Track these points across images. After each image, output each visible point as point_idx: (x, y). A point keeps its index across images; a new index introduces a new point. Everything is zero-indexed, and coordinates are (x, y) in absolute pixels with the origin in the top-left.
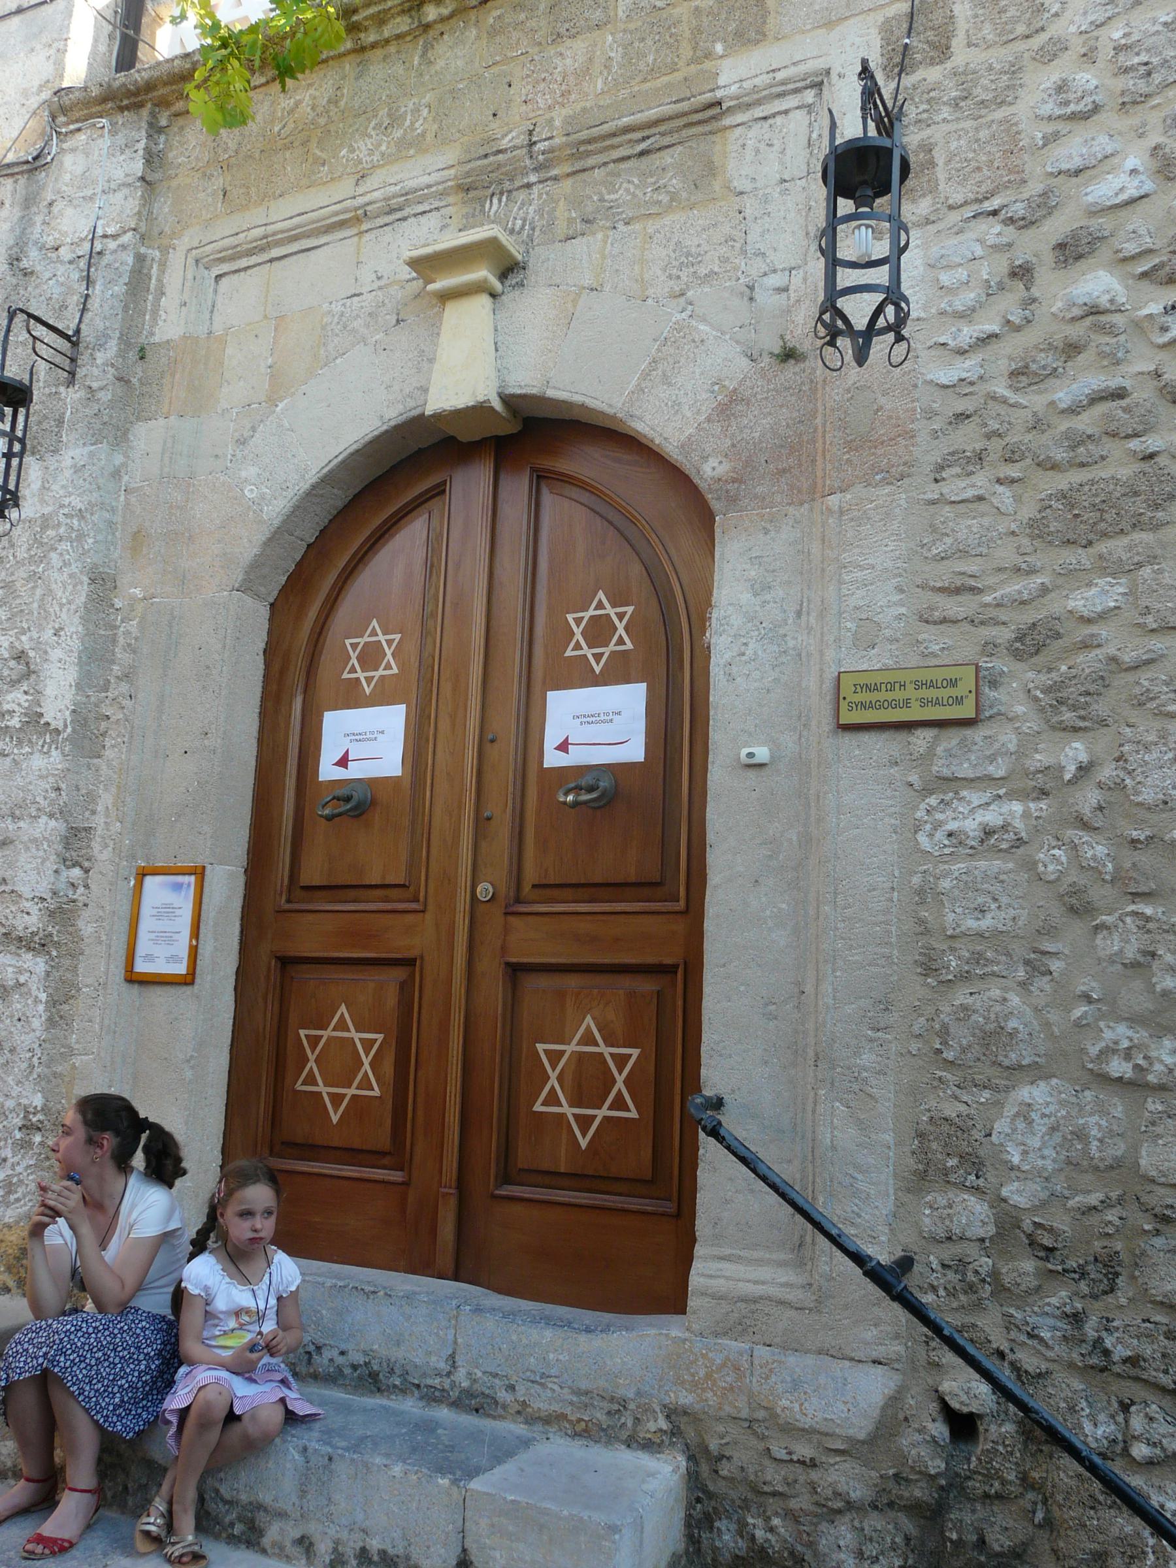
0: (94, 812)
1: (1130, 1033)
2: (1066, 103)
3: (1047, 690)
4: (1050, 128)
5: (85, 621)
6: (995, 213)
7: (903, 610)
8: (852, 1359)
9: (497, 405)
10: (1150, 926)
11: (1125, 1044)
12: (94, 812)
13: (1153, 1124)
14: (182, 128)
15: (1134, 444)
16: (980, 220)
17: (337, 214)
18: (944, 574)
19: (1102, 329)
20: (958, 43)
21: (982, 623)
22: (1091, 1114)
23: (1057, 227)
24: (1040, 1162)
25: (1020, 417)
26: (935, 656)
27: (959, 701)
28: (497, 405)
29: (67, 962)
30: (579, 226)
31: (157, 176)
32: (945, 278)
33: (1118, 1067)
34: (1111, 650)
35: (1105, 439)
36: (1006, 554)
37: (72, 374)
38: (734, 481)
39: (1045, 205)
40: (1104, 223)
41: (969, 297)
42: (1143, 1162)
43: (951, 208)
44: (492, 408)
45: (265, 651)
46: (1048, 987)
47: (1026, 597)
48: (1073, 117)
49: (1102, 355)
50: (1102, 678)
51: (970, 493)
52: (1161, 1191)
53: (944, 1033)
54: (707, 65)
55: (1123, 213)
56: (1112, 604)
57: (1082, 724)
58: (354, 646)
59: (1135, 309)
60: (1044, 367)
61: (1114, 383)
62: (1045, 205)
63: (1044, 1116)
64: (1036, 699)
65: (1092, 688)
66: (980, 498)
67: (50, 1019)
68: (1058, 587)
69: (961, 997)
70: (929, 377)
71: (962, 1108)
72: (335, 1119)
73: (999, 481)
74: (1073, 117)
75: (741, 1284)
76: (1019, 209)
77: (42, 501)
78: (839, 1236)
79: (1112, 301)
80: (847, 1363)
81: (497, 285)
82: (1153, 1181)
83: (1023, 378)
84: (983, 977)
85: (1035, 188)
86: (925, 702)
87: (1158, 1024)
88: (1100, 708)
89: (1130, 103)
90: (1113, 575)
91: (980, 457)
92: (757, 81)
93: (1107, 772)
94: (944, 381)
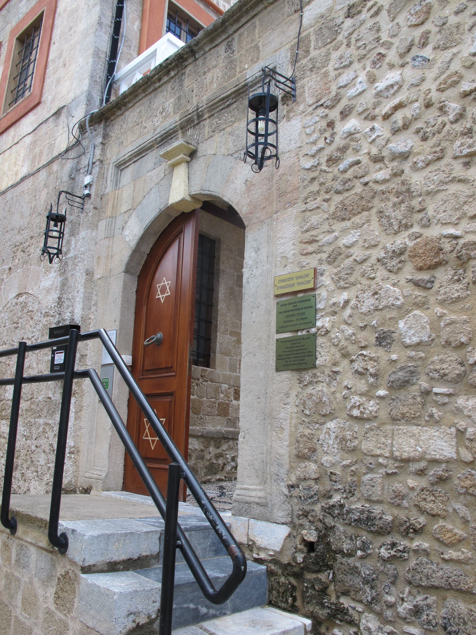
0: (87, 350)
1: (360, 399)
2: (342, 63)
3: (336, 274)
4: (336, 72)
5: (85, 288)
6: (322, 105)
7: (294, 252)
8: (276, 523)
9: (188, 198)
10: (366, 358)
11: (358, 404)
12: (87, 350)
13: (367, 433)
14: (113, 125)
15: (362, 180)
16: (318, 108)
17: (149, 143)
18: (307, 236)
19: (352, 140)
20: (312, 49)
21: (319, 253)
22: (348, 431)
23: (340, 107)
24: (333, 450)
25: (330, 176)
26: (305, 267)
27: (309, 282)
28: (188, 198)
29: (80, 399)
30: (211, 134)
31: (106, 141)
32: (308, 131)
33: (356, 413)
34: (354, 257)
35: (354, 179)
36: (326, 227)
37: (82, 209)
38: (251, 213)
39: (337, 99)
40: (354, 102)
41: (314, 136)
42: (362, 447)
43: (309, 106)
44: (187, 201)
45: (136, 292)
46: (335, 385)
47: (330, 241)
48: (345, 67)
49: (354, 149)
50: (352, 267)
51: (315, 206)
52: (368, 458)
53: (304, 404)
54: (244, 72)
55: (359, 98)
56: (355, 240)
57: (346, 286)
58: (159, 286)
59: (363, 131)
60: (336, 157)
61: (356, 159)
62: (337, 99)
63: (334, 432)
64: (333, 278)
65: (349, 272)
66: (318, 208)
67: (75, 418)
68: (341, 236)
69: (310, 390)
70: (303, 166)
71: (310, 431)
72: (153, 448)
73: (324, 201)
74: (345, 67)
75: (247, 498)
76: (329, 103)
77: (75, 251)
78: (190, 455)
79: (355, 129)
80: (275, 524)
81: (189, 159)
82: (366, 455)
83: (331, 162)
84: (316, 382)
85: (334, 93)
86: (299, 284)
87: (370, 396)
88: (352, 279)
89: (361, 58)
90: (356, 229)
91: (318, 192)
92: (257, 75)
93: (353, 302)
94: (307, 167)
